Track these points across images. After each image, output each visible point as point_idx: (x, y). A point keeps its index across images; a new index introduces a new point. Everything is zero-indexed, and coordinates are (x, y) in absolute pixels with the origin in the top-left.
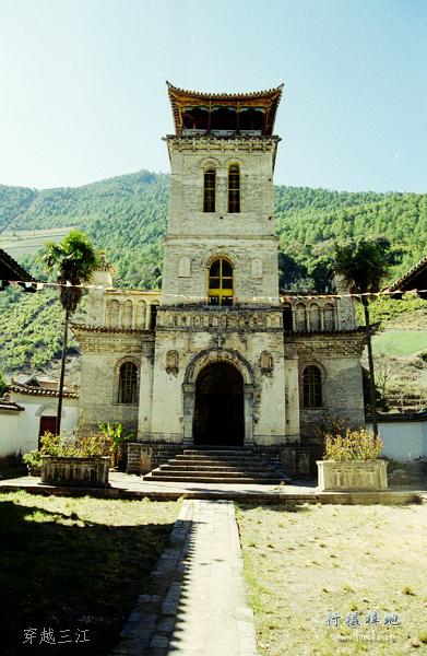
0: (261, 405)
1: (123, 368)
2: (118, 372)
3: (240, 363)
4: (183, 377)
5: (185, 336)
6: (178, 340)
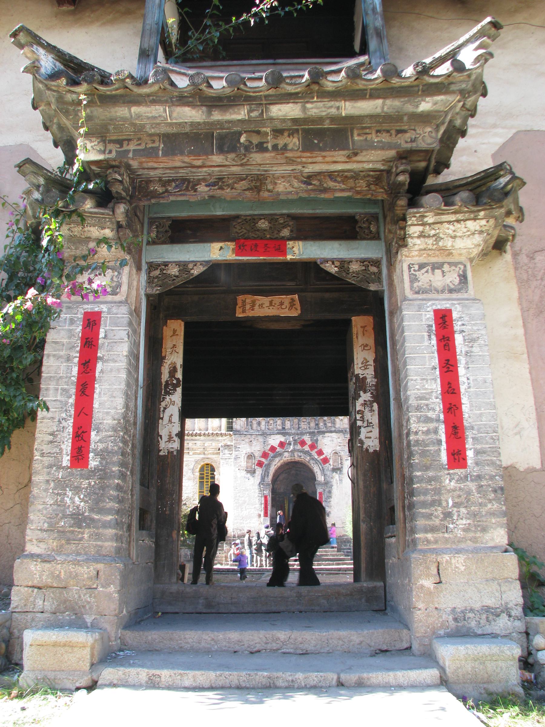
0: (332, 499)
1: (202, 469)
2: (197, 474)
3: (312, 462)
4: (260, 477)
5: (261, 439)
6: (254, 443)
